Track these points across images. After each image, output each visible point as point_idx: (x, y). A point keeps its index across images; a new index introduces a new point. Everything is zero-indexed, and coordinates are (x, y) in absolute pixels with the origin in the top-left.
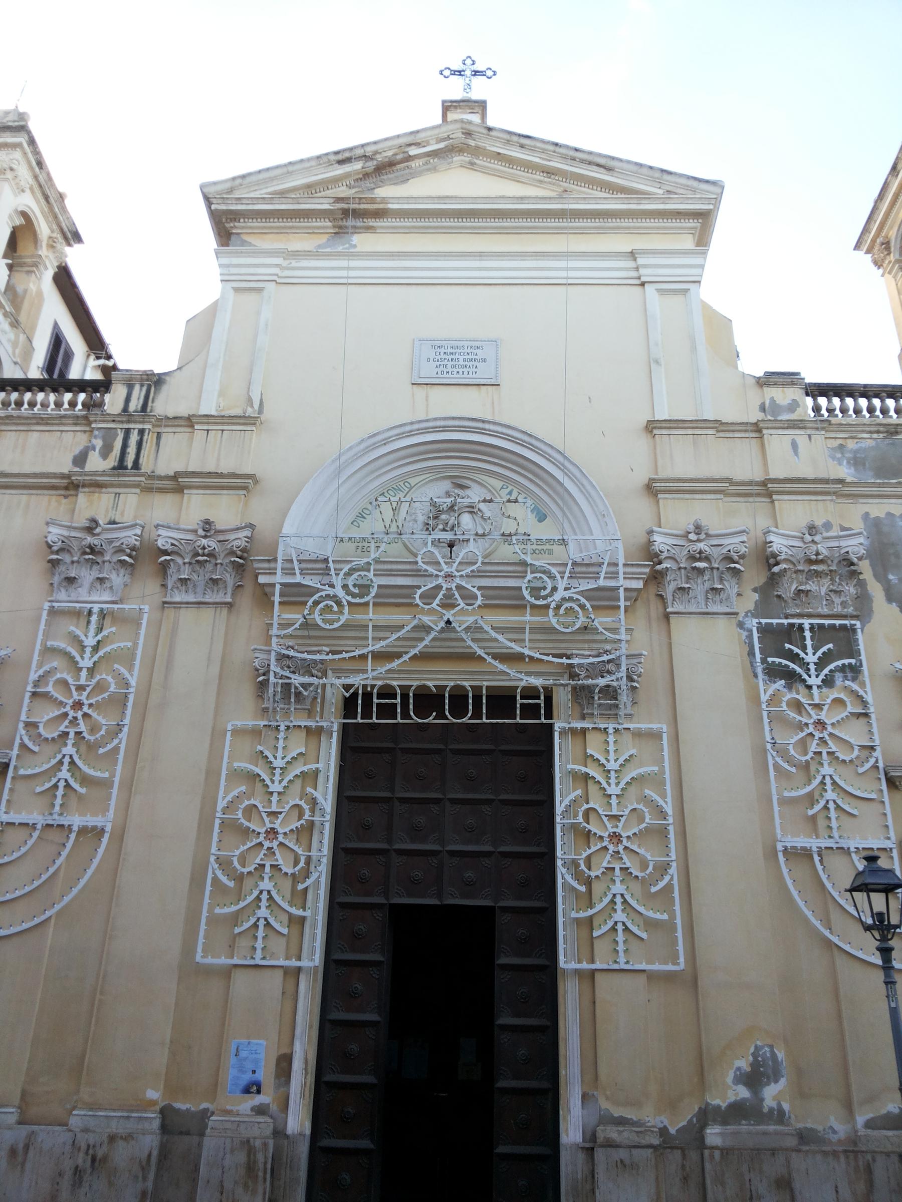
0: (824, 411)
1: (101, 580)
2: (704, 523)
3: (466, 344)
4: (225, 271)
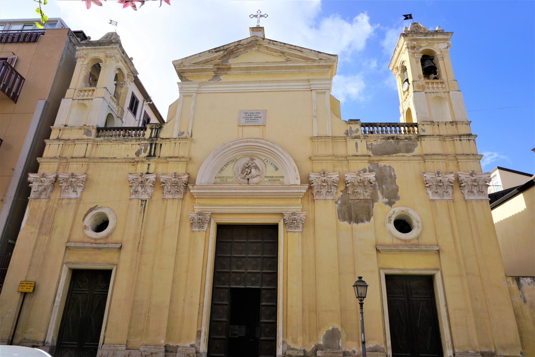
3: (255, 112)
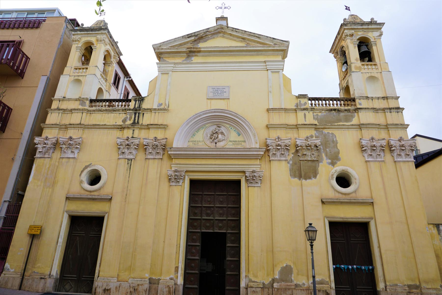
0: (314, 105)
1: (130, 153)
2: (280, 137)
4: (159, 66)
